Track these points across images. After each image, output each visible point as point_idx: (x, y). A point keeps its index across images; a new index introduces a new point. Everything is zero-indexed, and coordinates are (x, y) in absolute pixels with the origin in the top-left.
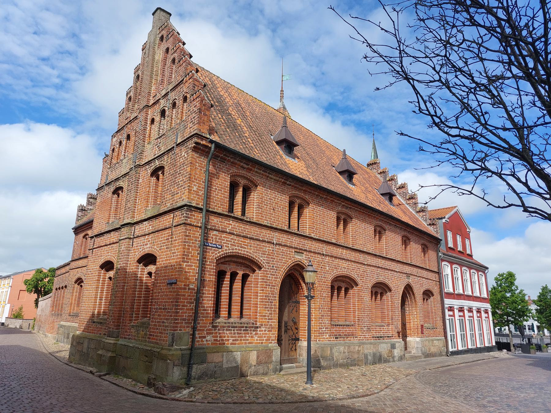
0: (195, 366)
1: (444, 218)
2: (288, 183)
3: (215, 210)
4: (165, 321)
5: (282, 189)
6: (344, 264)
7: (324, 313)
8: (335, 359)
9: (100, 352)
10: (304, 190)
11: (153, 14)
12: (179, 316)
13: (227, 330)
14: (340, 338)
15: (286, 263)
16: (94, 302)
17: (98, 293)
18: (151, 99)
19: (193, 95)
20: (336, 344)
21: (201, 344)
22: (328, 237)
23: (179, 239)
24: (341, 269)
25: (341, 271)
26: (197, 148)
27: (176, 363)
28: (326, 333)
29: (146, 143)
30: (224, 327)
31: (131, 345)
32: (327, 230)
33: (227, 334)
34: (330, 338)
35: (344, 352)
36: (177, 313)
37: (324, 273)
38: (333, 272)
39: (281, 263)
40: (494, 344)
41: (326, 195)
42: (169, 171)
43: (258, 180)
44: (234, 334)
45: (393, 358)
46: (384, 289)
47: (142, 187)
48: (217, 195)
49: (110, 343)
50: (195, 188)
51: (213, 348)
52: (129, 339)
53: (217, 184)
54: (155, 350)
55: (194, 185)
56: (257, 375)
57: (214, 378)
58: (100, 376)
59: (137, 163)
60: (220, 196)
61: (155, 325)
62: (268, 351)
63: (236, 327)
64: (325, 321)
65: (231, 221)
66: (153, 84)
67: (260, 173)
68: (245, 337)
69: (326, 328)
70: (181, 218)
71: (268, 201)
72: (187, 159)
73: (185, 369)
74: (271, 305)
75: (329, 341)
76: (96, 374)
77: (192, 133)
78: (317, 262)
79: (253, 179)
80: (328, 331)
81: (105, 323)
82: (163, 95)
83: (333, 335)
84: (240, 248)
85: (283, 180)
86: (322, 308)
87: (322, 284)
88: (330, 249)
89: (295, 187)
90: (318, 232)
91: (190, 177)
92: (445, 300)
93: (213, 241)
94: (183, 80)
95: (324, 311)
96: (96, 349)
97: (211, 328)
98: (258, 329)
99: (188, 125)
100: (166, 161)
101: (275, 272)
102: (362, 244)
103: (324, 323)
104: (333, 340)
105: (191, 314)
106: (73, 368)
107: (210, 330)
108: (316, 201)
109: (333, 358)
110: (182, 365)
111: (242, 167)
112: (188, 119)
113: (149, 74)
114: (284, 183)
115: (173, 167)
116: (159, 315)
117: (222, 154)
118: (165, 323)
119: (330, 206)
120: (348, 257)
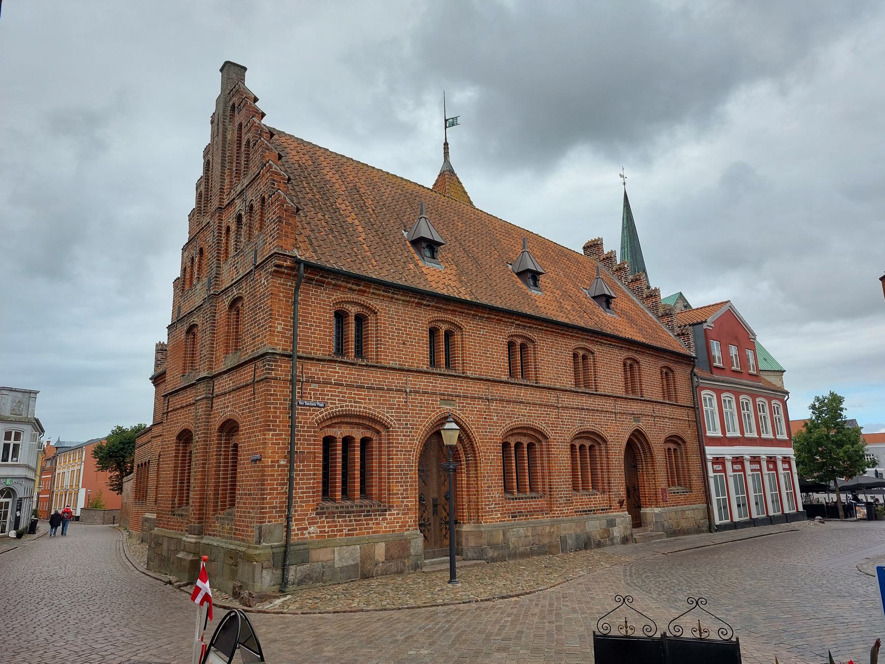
0: (293, 568)
1: (706, 322)
2: (425, 303)
3: (313, 355)
4: (251, 510)
5: (416, 312)
7: (492, 483)
8: (511, 546)
9: (180, 555)
10: (452, 310)
11: (221, 70)
12: (267, 503)
13: (338, 517)
14: (520, 516)
15: (427, 418)
16: (173, 487)
17: (177, 473)
18: (225, 197)
19: (271, 197)
20: (512, 525)
22: (495, 373)
23: (262, 400)
24: (517, 418)
25: (518, 421)
26: (278, 272)
27: (265, 565)
28: (495, 511)
29: (222, 262)
30: (334, 513)
31: (215, 544)
32: (493, 364)
33: (339, 522)
34: (502, 518)
35: (526, 536)
36: (264, 499)
37: (489, 425)
38: (504, 423)
39: (419, 417)
40: (801, 509)
41: (488, 314)
42: (249, 304)
43: (377, 305)
44: (351, 521)
45: (612, 540)
46: (595, 440)
47: (220, 325)
48: (314, 333)
49: (191, 543)
50: (279, 328)
51: (318, 542)
52: (214, 535)
53: (313, 318)
54: (240, 549)
55: (279, 324)
56: (386, 574)
57: (323, 582)
58: (179, 587)
59: (212, 292)
60: (319, 334)
61: (241, 516)
62: (403, 542)
63: (353, 512)
64: (493, 494)
66: (225, 176)
67: (379, 295)
68: (367, 524)
69: (496, 504)
70: (263, 371)
71: (394, 332)
72: (267, 288)
73: (279, 572)
74: (406, 478)
75: (502, 521)
76: (175, 584)
77: (273, 252)
78: (477, 411)
79: (370, 304)
80: (498, 507)
81: (187, 515)
82: (238, 193)
83: (508, 513)
84: (353, 404)
85: (416, 300)
86: (489, 476)
87: (488, 442)
88: (500, 390)
89: (437, 307)
90: (478, 368)
91: (271, 314)
92: (707, 448)
93: (311, 398)
94: (259, 173)
95: (491, 480)
96: (177, 551)
97: (314, 516)
98: (387, 513)
99: (267, 239)
100: (244, 290)
101: (411, 432)
102: (552, 379)
103: (492, 497)
104: (507, 521)
105: (284, 500)
106: (151, 579)
107: (313, 518)
108: (473, 324)
109: (508, 544)
111: (350, 289)
112: (267, 230)
113: (220, 161)
114: (419, 304)
115: (252, 298)
116: (245, 503)
117: (317, 275)
118: (251, 513)
119: (496, 328)
120: (529, 398)
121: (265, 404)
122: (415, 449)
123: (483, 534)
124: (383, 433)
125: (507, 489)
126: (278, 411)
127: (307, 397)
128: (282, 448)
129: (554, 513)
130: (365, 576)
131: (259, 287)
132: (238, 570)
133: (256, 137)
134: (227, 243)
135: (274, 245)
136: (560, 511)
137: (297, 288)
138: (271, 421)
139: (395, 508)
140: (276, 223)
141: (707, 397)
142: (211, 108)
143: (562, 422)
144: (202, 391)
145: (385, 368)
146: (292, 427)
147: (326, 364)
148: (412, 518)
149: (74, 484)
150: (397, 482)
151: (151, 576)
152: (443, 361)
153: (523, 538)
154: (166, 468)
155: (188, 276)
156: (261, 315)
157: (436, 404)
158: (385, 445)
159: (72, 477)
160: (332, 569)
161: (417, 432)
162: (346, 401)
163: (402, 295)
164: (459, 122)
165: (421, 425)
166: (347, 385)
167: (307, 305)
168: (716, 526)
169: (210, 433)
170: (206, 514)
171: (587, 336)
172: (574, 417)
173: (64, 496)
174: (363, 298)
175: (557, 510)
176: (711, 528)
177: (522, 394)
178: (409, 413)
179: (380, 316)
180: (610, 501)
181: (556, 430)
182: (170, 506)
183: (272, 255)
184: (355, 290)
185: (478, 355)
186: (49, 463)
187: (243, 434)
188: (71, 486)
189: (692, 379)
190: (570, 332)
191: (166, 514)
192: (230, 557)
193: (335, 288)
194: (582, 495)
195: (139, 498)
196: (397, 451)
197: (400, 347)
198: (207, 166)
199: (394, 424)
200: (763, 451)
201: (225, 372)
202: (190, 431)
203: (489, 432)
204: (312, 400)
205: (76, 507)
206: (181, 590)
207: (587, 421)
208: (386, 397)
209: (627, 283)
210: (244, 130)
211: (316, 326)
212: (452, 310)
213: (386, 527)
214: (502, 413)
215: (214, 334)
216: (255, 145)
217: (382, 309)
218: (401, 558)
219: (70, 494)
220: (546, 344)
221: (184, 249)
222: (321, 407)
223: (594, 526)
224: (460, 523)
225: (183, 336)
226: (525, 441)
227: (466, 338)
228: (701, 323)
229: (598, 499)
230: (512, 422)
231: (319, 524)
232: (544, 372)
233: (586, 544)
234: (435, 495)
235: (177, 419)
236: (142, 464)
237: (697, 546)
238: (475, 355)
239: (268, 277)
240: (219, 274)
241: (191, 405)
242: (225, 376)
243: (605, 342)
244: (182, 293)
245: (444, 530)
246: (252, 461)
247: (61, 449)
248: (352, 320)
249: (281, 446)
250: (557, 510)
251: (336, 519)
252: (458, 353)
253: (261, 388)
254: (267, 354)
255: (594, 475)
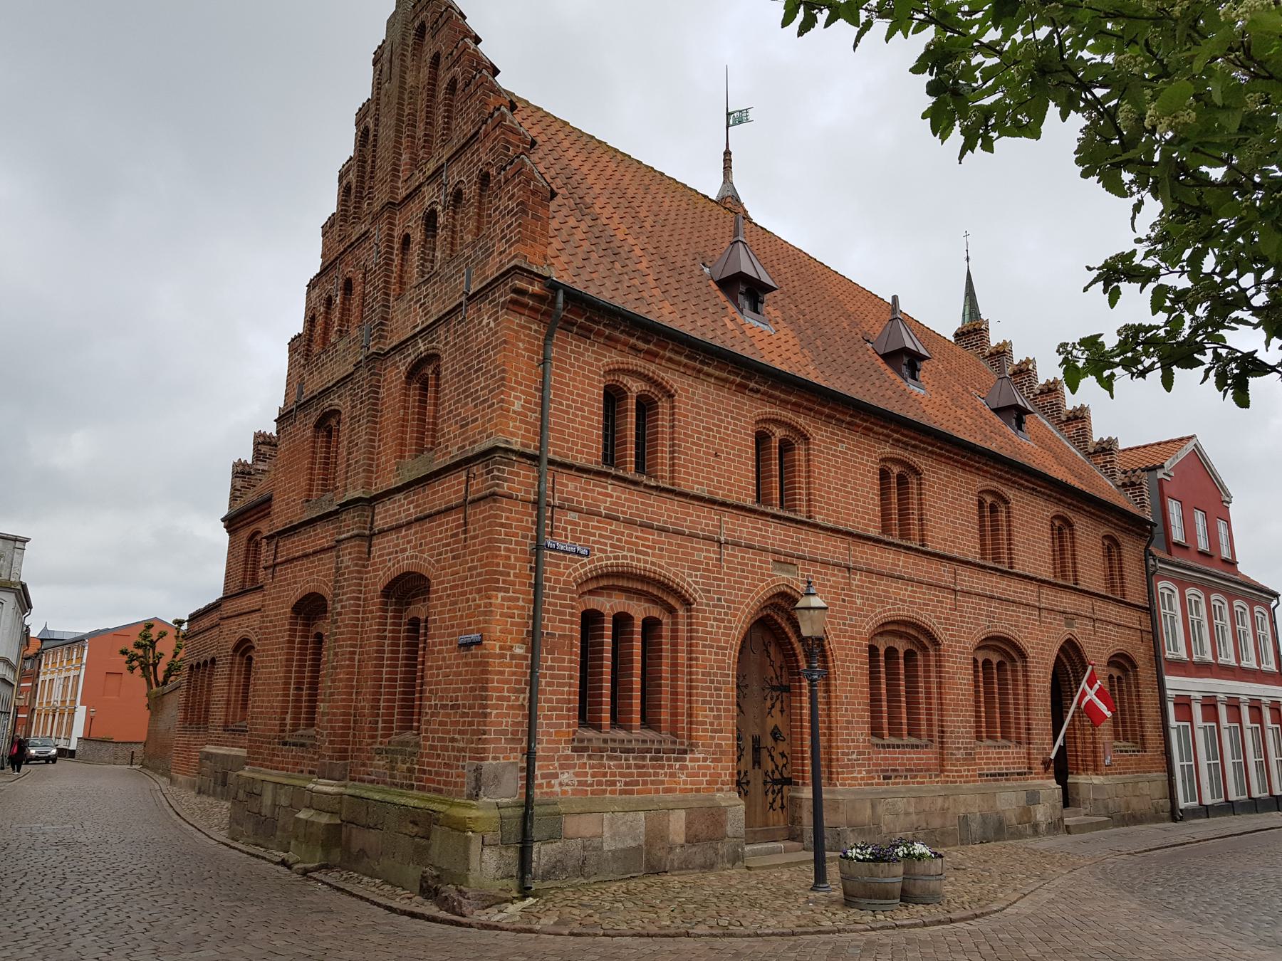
1: (1162, 466)
2: (752, 385)
3: (569, 461)
4: (456, 736)
5: (737, 401)
6: (905, 591)
8: (884, 829)
13: (610, 758)
14: (896, 777)
15: (751, 591)
18: (400, 185)
19: (504, 169)
21: (547, 793)
22: (859, 523)
23: (483, 535)
24: (893, 604)
28: (859, 765)
29: (392, 299)
33: (610, 768)
34: (870, 778)
35: (907, 814)
37: (849, 614)
39: (740, 590)
41: (851, 416)
42: (453, 365)
43: (675, 381)
44: (629, 767)
45: (1035, 827)
48: (573, 421)
55: (516, 398)
63: (633, 751)
65: (610, 487)
69: (859, 754)
73: (512, 854)
79: (663, 379)
80: (863, 759)
82: (428, 174)
84: (634, 554)
85: (738, 380)
86: (848, 704)
87: (847, 643)
91: (503, 379)
92: (1167, 678)
93: (566, 537)
97: (569, 752)
98: (688, 756)
103: (853, 741)
105: (520, 719)
107: (567, 757)
108: (826, 431)
109: (879, 826)
110: (505, 844)
111: (633, 348)
113: (393, 122)
114: (742, 388)
117: (581, 317)
119: (862, 443)
120: (912, 572)
121: (490, 540)
122: (732, 645)
123: (841, 806)
124: (681, 613)
125: (876, 731)
126: (512, 556)
127: (561, 535)
128: (517, 624)
129: (948, 776)
130: (655, 870)
131: (477, 332)
132: (431, 845)
133: (470, 73)
134: (402, 265)
135: (510, 254)
136: (957, 771)
137: (549, 336)
138: (501, 573)
139: (701, 748)
140: (514, 215)
141: (1166, 592)
142: (379, 35)
143: (961, 616)
144: (351, 524)
145: (685, 495)
146: (537, 586)
147: (593, 480)
148: (726, 769)
149: (68, 698)
150: (704, 702)
151: (240, 850)
152: (776, 493)
153: (902, 817)
154: (270, 661)
155: (318, 330)
156: (480, 383)
157: (767, 569)
158: (683, 634)
159: (65, 687)
160: (599, 853)
161: (735, 616)
162: (622, 548)
163: (716, 368)
164: (750, 118)
165: (742, 603)
166: (626, 521)
167: (562, 369)
168: (1181, 810)
169: (365, 599)
170: (355, 743)
171: (1001, 471)
172: (980, 609)
173: (51, 718)
174: (653, 367)
175: (951, 771)
176: (1175, 815)
177: (901, 564)
178: (723, 580)
179: (679, 402)
180: (1029, 759)
181: (953, 630)
182: (277, 728)
183: (508, 271)
184: (640, 351)
185: (834, 489)
186: (28, 665)
187: (440, 598)
188: (63, 702)
189: (1146, 560)
190: (976, 462)
191: (270, 743)
192: (411, 822)
193: (609, 343)
194: (989, 747)
195: (192, 721)
196: (704, 646)
197: (708, 460)
198: (365, 138)
199: (700, 596)
200: (1245, 689)
201: (398, 490)
202: (323, 598)
203: (850, 625)
204: (569, 541)
205: (70, 734)
206: (311, 877)
207: (998, 618)
208: (687, 547)
209: (1031, 396)
210: (443, 64)
211: (577, 409)
212: (795, 404)
213: (685, 783)
214: (870, 594)
215: (376, 423)
216: (467, 85)
217: (682, 389)
218: (710, 839)
219: (62, 714)
220: (938, 478)
221: (312, 286)
222: (583, 555)
223: (1008, 801)
224: (797, 784)
225: (309, 433)
226: (901, 646)
227: (814, 455)
228: (1154, 469)
229: (1011, 756)
230: (885, 611)
231: (577, 770)
232: (935, 527)
233: (997, 830)
234: (757, 732)
235: (295, 577)
236: (198, 664)
237: (1173, 841)
238: (829, 487)
239: (497, 312)
240: (387, 320)
241: (324, 550)
242: (400, 496)
243: (1026, 484)
244: (306, 360)
245: (770, 793)
246: (461, 645)
247: (50, 643)
248: (632, 404)
249: (517, 620)
250: (951, 771)
251: (605, 761)
252: (799, 482)
253: (478, 514)
254: (495, 449)
255: (1004, 713)
